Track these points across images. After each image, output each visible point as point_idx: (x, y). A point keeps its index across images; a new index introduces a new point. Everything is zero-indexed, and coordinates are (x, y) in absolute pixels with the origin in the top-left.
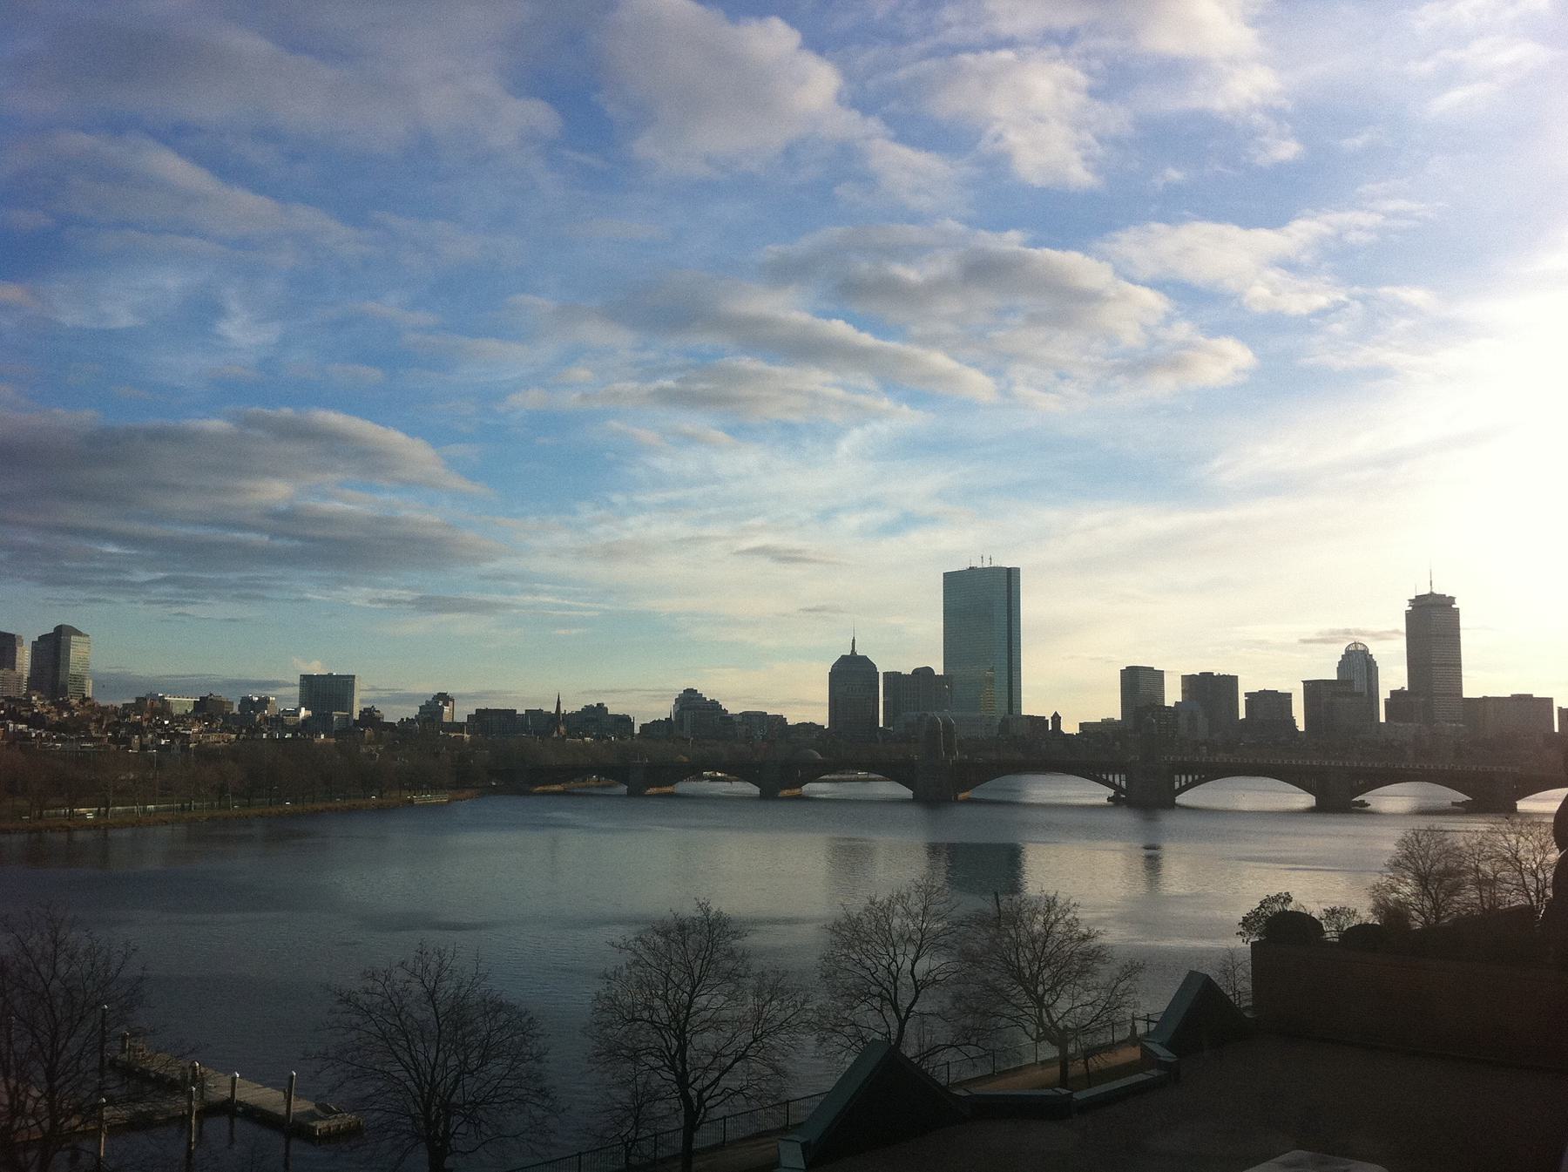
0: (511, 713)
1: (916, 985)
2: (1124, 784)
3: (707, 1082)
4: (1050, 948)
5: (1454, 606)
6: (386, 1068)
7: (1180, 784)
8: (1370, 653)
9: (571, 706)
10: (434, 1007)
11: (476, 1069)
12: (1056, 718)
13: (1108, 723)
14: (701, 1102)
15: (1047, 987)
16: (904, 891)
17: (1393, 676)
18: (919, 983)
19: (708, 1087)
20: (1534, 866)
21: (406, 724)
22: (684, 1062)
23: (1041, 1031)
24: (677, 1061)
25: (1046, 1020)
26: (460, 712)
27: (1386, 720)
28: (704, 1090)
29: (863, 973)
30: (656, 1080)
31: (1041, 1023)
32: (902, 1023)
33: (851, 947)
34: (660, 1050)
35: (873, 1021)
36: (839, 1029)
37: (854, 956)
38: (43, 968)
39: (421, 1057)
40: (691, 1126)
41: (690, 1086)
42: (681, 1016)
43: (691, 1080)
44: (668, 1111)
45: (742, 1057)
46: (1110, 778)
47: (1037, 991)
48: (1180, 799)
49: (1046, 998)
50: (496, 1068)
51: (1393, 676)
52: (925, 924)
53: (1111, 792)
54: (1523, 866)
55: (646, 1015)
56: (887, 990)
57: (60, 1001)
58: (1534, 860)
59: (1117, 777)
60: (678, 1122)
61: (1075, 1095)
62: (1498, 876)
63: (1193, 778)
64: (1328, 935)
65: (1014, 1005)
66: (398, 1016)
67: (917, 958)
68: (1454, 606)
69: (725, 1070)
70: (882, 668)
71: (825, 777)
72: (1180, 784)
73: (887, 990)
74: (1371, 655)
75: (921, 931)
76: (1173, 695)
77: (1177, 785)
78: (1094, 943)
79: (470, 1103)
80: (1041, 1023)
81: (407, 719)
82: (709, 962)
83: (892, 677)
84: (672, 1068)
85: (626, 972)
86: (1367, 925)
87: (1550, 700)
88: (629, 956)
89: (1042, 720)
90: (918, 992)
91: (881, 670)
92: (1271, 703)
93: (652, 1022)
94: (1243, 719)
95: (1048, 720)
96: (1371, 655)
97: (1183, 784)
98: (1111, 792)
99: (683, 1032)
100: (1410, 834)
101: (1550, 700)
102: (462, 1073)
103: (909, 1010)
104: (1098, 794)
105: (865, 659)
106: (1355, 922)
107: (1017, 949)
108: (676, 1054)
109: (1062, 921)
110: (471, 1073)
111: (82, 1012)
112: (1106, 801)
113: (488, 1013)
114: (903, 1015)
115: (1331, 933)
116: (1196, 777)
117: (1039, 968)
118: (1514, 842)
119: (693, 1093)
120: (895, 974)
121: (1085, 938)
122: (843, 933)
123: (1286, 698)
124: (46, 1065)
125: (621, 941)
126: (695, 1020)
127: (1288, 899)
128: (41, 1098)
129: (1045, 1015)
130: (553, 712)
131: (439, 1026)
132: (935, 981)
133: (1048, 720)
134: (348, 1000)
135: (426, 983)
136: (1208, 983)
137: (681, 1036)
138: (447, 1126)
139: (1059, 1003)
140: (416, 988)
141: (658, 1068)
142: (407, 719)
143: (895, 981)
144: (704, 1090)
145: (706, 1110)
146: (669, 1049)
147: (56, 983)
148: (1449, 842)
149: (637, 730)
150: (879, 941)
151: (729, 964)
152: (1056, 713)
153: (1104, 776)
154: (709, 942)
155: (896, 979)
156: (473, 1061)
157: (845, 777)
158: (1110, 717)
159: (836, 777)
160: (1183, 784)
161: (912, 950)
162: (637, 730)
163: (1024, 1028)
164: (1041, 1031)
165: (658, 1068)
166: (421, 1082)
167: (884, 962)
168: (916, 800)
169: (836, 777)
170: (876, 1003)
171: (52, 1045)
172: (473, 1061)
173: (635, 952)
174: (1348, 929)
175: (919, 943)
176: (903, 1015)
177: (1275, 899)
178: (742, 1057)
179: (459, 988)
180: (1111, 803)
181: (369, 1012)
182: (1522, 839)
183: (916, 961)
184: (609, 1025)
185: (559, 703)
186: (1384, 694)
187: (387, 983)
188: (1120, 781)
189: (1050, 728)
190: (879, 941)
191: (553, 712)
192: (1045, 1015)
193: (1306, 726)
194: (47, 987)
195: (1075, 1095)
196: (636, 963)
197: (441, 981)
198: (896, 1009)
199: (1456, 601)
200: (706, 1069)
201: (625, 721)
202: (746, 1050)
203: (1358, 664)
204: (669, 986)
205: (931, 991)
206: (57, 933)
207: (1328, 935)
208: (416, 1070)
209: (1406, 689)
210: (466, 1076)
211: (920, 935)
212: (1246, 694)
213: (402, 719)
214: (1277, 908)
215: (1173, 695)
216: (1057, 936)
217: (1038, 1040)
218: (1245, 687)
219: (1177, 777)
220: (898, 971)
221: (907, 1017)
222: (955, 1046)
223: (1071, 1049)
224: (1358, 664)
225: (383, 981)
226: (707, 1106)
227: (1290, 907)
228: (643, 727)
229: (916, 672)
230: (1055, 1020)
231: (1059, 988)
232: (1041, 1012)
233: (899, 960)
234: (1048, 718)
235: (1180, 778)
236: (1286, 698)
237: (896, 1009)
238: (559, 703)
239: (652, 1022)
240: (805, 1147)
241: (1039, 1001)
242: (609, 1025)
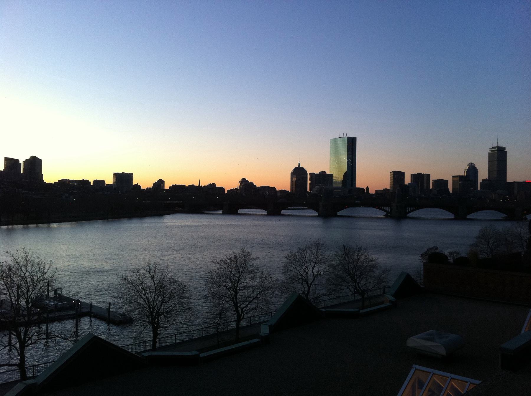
0: (184, 186)
1: (314, 276)
2: (389, 210)
3: (244, 306)
4: (360, 263)
5: (505, 151)
6: (139, 301)
7: (409, 210)
8: (476, 166)
9: (204, 184)
10: (154, 281)
11: (168, 301)
12: (368, 189)
13: (385, 190)
14: (242, 312)
15: (358, 276)
16: (310, 245)
17: (483, 174)
18: (315, 275)
19: (245, 307)
20: (526, 238)
21: (148, 190)
22: (236, 299)
23: (355, 290)
24: (234, 300)
25: (358, 287)
26: (167, 186)
27: (480, 189)
28: (243, 308)
29: (297, 272)
30: (227, 306)
31: (356, 288)
32: (309, 287)
33: (292, 263)
34: (229, 296)
35: (300, 288)
36: (288, 289)
37: (293, 266)
38: (23, 269)
39: (150, 298)
40: (239, 318)
41: (239, 307)
42: (236, 285)
43: (239, 305)
44: (231, 316)
45: (255, 298)
46: (385, 208)
47: (354, 278)
48: (408, 215)
49: (358, 280)
50: (174, 301)
51: (483, 174)
52: (317, 256)
53: (385, 213)
54: (522, 238)
55: (224, 284)
56: (304, 277)
57: (29, 279)
58: (526, 236)
59: (387, 208)
60: (235, 317)
61: (361, 311)
62: (513, 242)
63: (413, 208)
64: (449, 260)
65: (347, 282)
66: (142, 284)
67: (314, 267)
68: (505, 151)
69: (250, 302)
70: (309, 172)
71: (289, 208)
72: (409, 210)
73: (304, 277)
74: (476, 167)
75: (316, 258)
76: (408, 180)
77: (407, 211)
78: (374, 263)
79: (165, 312)
80: (356, 288)
81: (149, 188)
82: (245, 268)
83: (312, 174)
84: (233, 301)
85: (217, 271)
86: (463, 257)
87: (428, 176)
88: (218, 266)
89: (363, 189)
90: (314, 278)
91: (308, 172)
92: (441, 184)
93: (226, 287)
94: (431, 189)
95: (364, 189)
96: (476, 167)
97: (410, 210)
98: (385, 213)
99: (236, 290)
100: (484, 228)
101: (428, 176)
102: (163, 302)
103: (311, 283)
104: (381, 214)
105: (303, 168)
106: (459, 256)
107: (348, 264)
108: (234, 297)
109: (363, 255)
110: (166, 302)
111: (37, 283)
112: (383, 216)
113: (171, 284)
114: (309, 285)
115: (450, 260)
116: (414, 208)
117: (355, 270)
118: (520, 230)
119: (239, 309)
120: (307, 272)
121: (371, 261)
122: (290, 259)
123: (447, 182)
124: (25, 300)
125: (216, 261)
126: (241, 286)
127: (437, 248)
128: (24, 310)
129: (357, 285)
130: (198, 186)
131: (155, 287)
132: (320, 274)
133: (364, 189)
134: (125, 279)
135: (151, 273)
136: (408, 276)
137: (236, 291)
138: (158, 320)
139: (361, 282)
140: (148, 275)
141: (228, 301)
142: (149, 188)
143: (307, 274)
144: (243, 308)
145: (244, 315)
146: (232, 295)
147: (27, 274)
148: (497, 230)
149: (226, 192)
150: (302, 261)
151: (251, 269)
152: (368, 187)
153: (383, 208)
154: (244, 261)
155: (307, 273)
156: (166, 299)
157: (295, 208)
158: (386, 188)
159: (292, 208)
160: (410, 210)
161: (313, 264)
162: (226, 192)
163: (350, 289)
164: (355, 290)
165: (228, 301)
166: (150, 306)
167: (304, 268)
168: (319, 216)
169: (292, 208)
170: (301, 281)
171: (27, 293)
172: (166, 299)
173: (220, 264)
174: (456, 258)
175: (315, 262)
176: (309, 285)
177: (432, 249)
178: (255, 298)
179: (162, 275)
180: (385, 217)
181: (132, 283)
182: (522, 229)
183: (314, 268)
184: (212, 287)
185: (199, 183)
186: (480, 180)
187: (138, 274)
188: (388, 209)
189: (365, 192)
190: (302, 261)
191: (198, 186)
192: (357, 285)
193: (453, 191)
194: (25, 275)
195: (361, 311)
196: (221, 268)
197: (155, 273)
198: (307, 283)
199: (506, 149)
200: (244, 302)
201: (222, 189)
202: (257, 296)
203: (472, 170)
204: (232, 275)
205: (319, 277)
206: (27, 258)
207: (449, 260)
208: (148, 301)
209: (488, 179)
210: (164, 303)
211: (315, 259)
212: (433, 180)
213: (147, 188)
214: (433, 251)
215: (408, 180)
216: (362, 260)
217: (355, 293)
218: (433, 178)
219: (407, 208)
220: (308, 271)
221: (311, 286)
222: (327, 295)
223: (366, 296)
224: (472, 170)
225: (136, 273)
226: (244, 313)
227: (437, 251)
228: (228, 191)
229: (320, 173)
230: (360, 287)
231: (362, 277)
232: (356, 284)
233: (309, 267)
234: (365, 188)
235: (409, 208)
236: (447, 182)
237: (307, 283)
238: (199, 183)
239: (226, 287)
240: (270, 327)
241: (355, 281)
242: (212, 287)
